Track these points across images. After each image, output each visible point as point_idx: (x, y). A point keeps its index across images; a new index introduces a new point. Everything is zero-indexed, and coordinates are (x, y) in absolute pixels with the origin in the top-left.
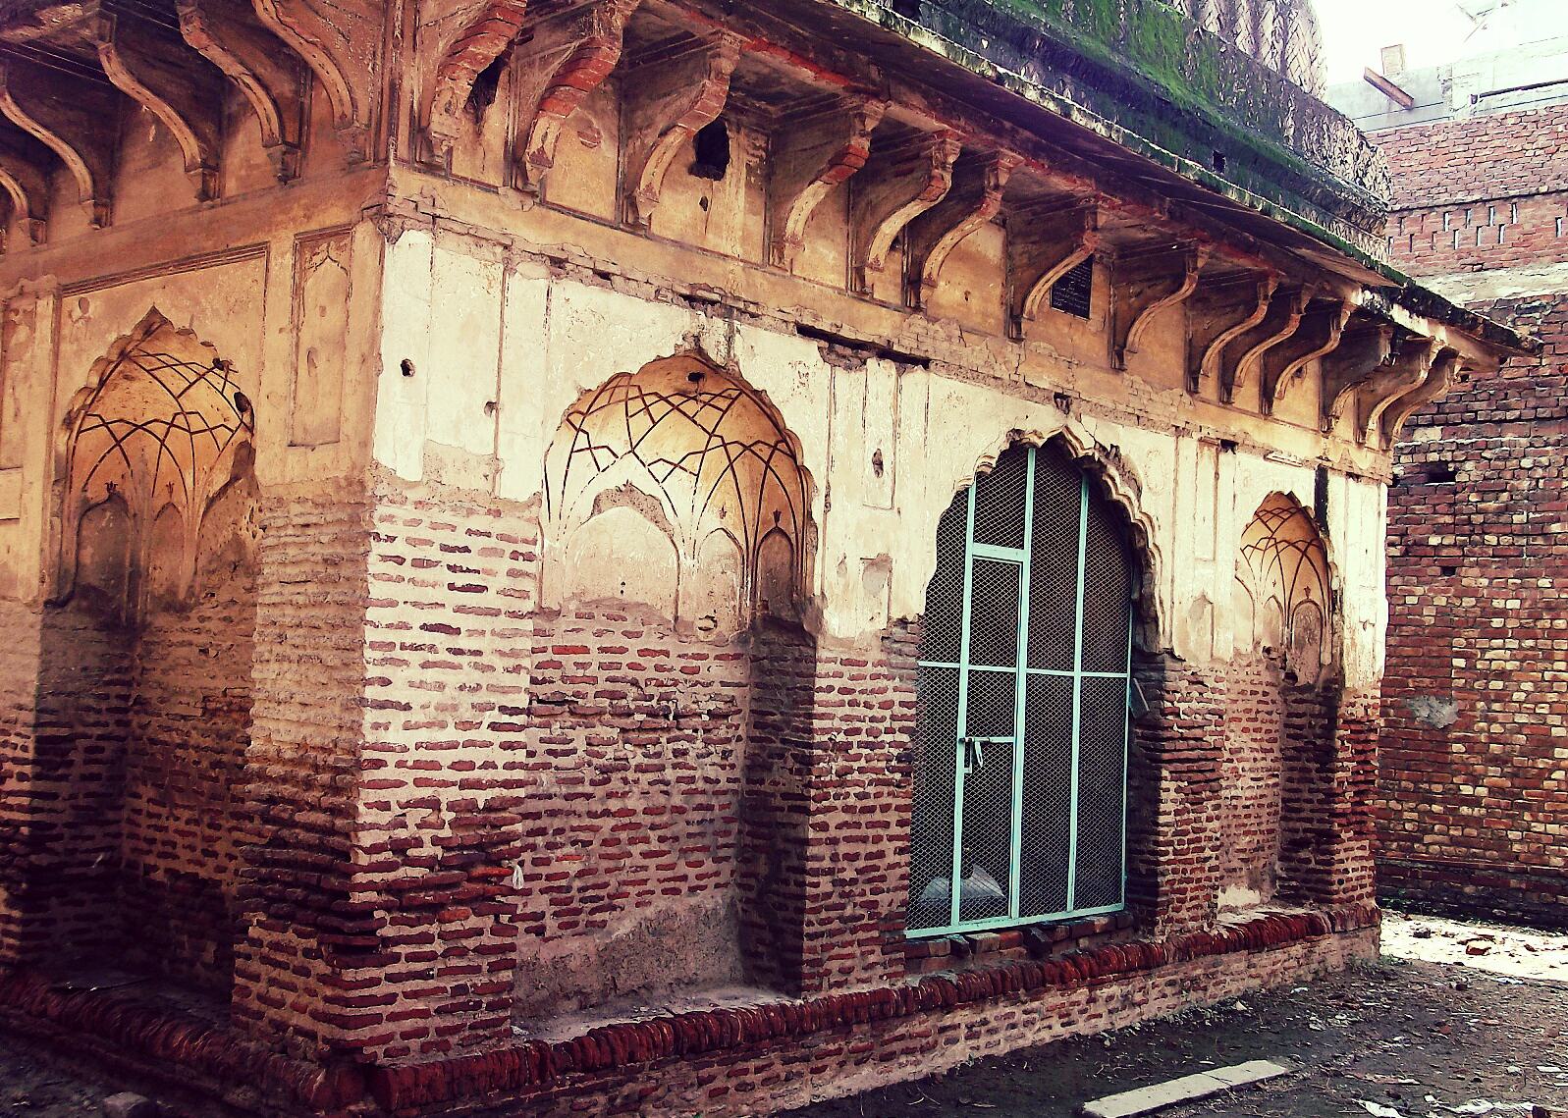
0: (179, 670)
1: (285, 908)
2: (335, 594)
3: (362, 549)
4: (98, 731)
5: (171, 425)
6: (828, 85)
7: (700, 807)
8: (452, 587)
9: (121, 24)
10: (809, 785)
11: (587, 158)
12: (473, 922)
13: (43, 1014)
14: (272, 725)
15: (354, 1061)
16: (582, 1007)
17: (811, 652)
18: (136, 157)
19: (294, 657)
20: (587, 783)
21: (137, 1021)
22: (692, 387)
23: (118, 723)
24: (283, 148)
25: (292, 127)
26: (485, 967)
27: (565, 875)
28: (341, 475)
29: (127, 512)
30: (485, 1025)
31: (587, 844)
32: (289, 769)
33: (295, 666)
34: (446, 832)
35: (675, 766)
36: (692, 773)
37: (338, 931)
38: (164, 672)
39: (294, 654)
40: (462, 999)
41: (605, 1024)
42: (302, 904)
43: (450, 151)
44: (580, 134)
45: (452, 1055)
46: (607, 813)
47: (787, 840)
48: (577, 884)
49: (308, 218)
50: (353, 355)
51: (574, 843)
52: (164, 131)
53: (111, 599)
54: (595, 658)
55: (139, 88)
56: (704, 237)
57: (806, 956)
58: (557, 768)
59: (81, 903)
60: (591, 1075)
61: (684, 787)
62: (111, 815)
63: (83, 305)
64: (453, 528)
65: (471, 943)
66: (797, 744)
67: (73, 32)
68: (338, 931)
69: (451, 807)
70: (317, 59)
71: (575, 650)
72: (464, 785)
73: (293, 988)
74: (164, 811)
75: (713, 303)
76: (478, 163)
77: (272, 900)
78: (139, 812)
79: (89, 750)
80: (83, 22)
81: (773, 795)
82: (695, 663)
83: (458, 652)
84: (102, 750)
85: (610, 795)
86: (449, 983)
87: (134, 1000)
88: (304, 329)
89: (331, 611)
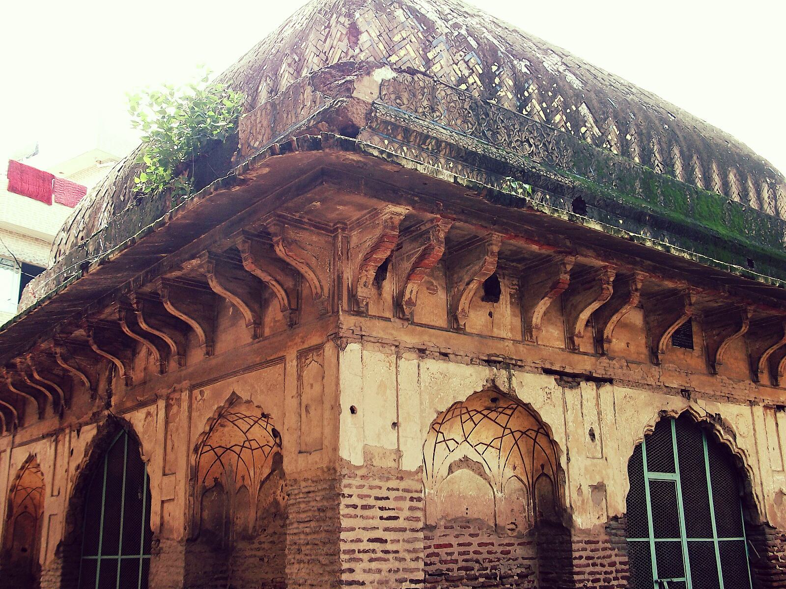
3: (336, 502)
5: (243, 447)
8: (381, 518)
18: (224, 322)
19: (306, 561)
22: (493, 405)
24: (290, 311)
33: (306, 565)
38: (243, 571)
43: (367, 304)
44: (428, 288)
50: (327, 406)
54: (456, 549)
56: (492, 331)
63: (202, 393)
64: (380, 488)
70: (303, 269)
76: (381, 308)
80: (200, 266)
82: (508, 548)
88: (303, 396)
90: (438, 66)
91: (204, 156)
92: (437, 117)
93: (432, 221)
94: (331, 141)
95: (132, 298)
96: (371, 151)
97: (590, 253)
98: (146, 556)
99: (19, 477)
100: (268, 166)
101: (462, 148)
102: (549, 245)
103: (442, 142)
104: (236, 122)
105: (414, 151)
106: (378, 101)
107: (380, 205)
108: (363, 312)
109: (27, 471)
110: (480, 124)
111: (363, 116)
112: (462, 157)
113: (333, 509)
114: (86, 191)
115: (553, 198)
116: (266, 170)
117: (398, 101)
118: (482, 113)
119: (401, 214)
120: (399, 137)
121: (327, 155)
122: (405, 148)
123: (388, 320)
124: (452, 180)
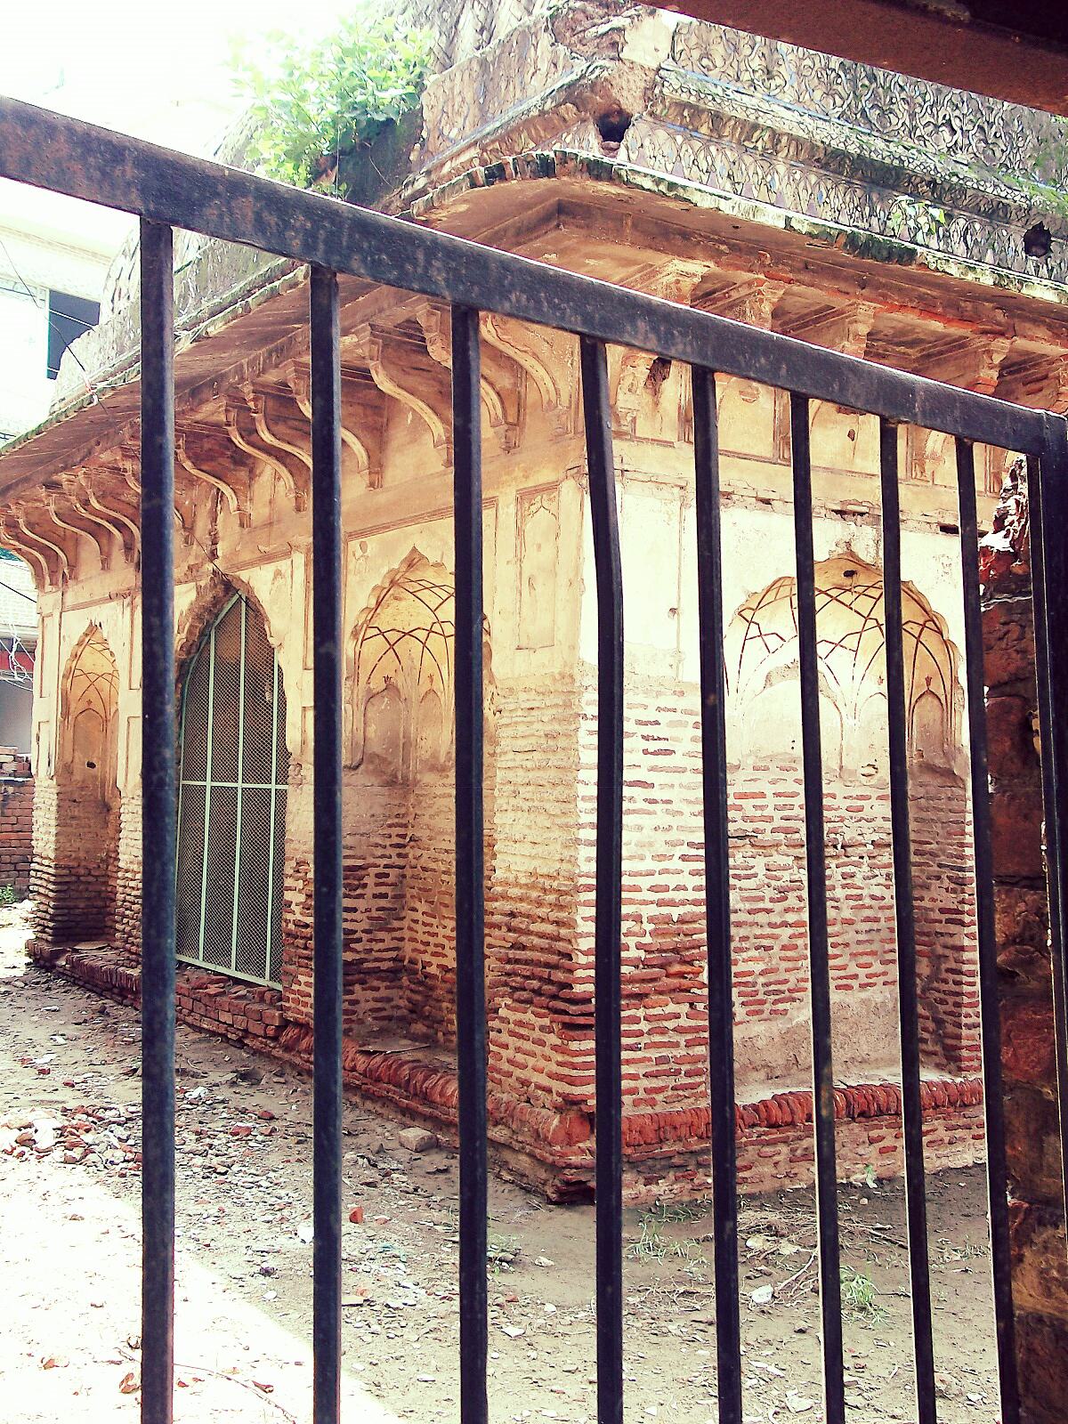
0: (442, 816)
1: (525, 995)
2: (554, 760)
3: (573, 727)
4: (386, 861)
5: (431, 631)
6: (956, 330)
7: (867, 919)
8: (646, 752)
9: (385, 346)
10: (963, 902)
11: (748, 409)
12: (672, 1008)
13: (353, 1069)
14: (510, 859)
15: (581, 1110)
16: (769, 1078)
17: (961, 792)
18: (398, 436)
19: (526, 808)
20: (767, 900)
21: (420, 1077)
22: (847, 582)
23: (399, 855)
24: (506, 427)
25: (512, 412)
26: (683, 1043)
27: (751, 973)
28: (556, 671)
29: (400, 697)
30: (685, 1087)
31: (768, 949)
32: (523, 891)
33: (526, 814)
34: (647, 940)
35: (844, 887)
36: (859, 892)
37: (565, 1012)
38: (431, 817)
39: (526, 805)
40: (665, 1067)
41: (787, 1091)
42: (538, 992)
43: (634, 420)
44: (741, 393)
45: (658, 1109)
46: (785, 924)
47: (945, 947)
48: (762, 980)
49: (527, 477)
50: (563, 580)
51: (757, 948)
52: (418, 418)
53: (390, 763)
54: (771, 801)
55: (400, 391)
56: (852, 462)
57: (964, 1043)
58: (741, 889)
59: (377, 989)
60: (775, 1130)
61: (852, 903)
62: (396, 924)
63: (363, 546)
64: (646, 707)
65: (671, 1024)
66: (952, 868)
67: (351, 351)
68: (565, 1012)
69: (651, 920)
70: (528, 362)
71: (754, 796)
72: (660, 903)
73: (533, 1055)
74: (434, 921)
75: (862, 514)
76: (657, 426)
77: (515, 989)
78: (416, 922)
79: (378, 876)
80: (358, 345)
81: (932, 910)
82: (860, 803)
83: (654, 802)
84: (387, 875)
85: (787, 910)
86: (654, 1054)
87: (418, 1061)
88: (524, 561)
89: (552, 774)
91: (363, 146)
92: (777, 87)
93: (750, 284)
94: (571, 164)
95: (246, 390)
96: (639, 180)
97: (1042, 332)
98: (279, 787)
99: (76, 656)
100: (465, 201)
101: (819, 144)
102: (962, 320)
104: (420, 86)
105: (728, 153)
106: (669, 64)
107: (658, 259)
108: (626, 434)
109: (88, 648)
111: (639, 93)
112: (818, 160)
113: (568, 736)
115: (988, 228)
116: (463, 208)
117: (705, 62)
119: (695, 275)
120: (704, 130)
121: (565, 183)
122: (713, 149)
123: (669, 444)
124: (781, 225)
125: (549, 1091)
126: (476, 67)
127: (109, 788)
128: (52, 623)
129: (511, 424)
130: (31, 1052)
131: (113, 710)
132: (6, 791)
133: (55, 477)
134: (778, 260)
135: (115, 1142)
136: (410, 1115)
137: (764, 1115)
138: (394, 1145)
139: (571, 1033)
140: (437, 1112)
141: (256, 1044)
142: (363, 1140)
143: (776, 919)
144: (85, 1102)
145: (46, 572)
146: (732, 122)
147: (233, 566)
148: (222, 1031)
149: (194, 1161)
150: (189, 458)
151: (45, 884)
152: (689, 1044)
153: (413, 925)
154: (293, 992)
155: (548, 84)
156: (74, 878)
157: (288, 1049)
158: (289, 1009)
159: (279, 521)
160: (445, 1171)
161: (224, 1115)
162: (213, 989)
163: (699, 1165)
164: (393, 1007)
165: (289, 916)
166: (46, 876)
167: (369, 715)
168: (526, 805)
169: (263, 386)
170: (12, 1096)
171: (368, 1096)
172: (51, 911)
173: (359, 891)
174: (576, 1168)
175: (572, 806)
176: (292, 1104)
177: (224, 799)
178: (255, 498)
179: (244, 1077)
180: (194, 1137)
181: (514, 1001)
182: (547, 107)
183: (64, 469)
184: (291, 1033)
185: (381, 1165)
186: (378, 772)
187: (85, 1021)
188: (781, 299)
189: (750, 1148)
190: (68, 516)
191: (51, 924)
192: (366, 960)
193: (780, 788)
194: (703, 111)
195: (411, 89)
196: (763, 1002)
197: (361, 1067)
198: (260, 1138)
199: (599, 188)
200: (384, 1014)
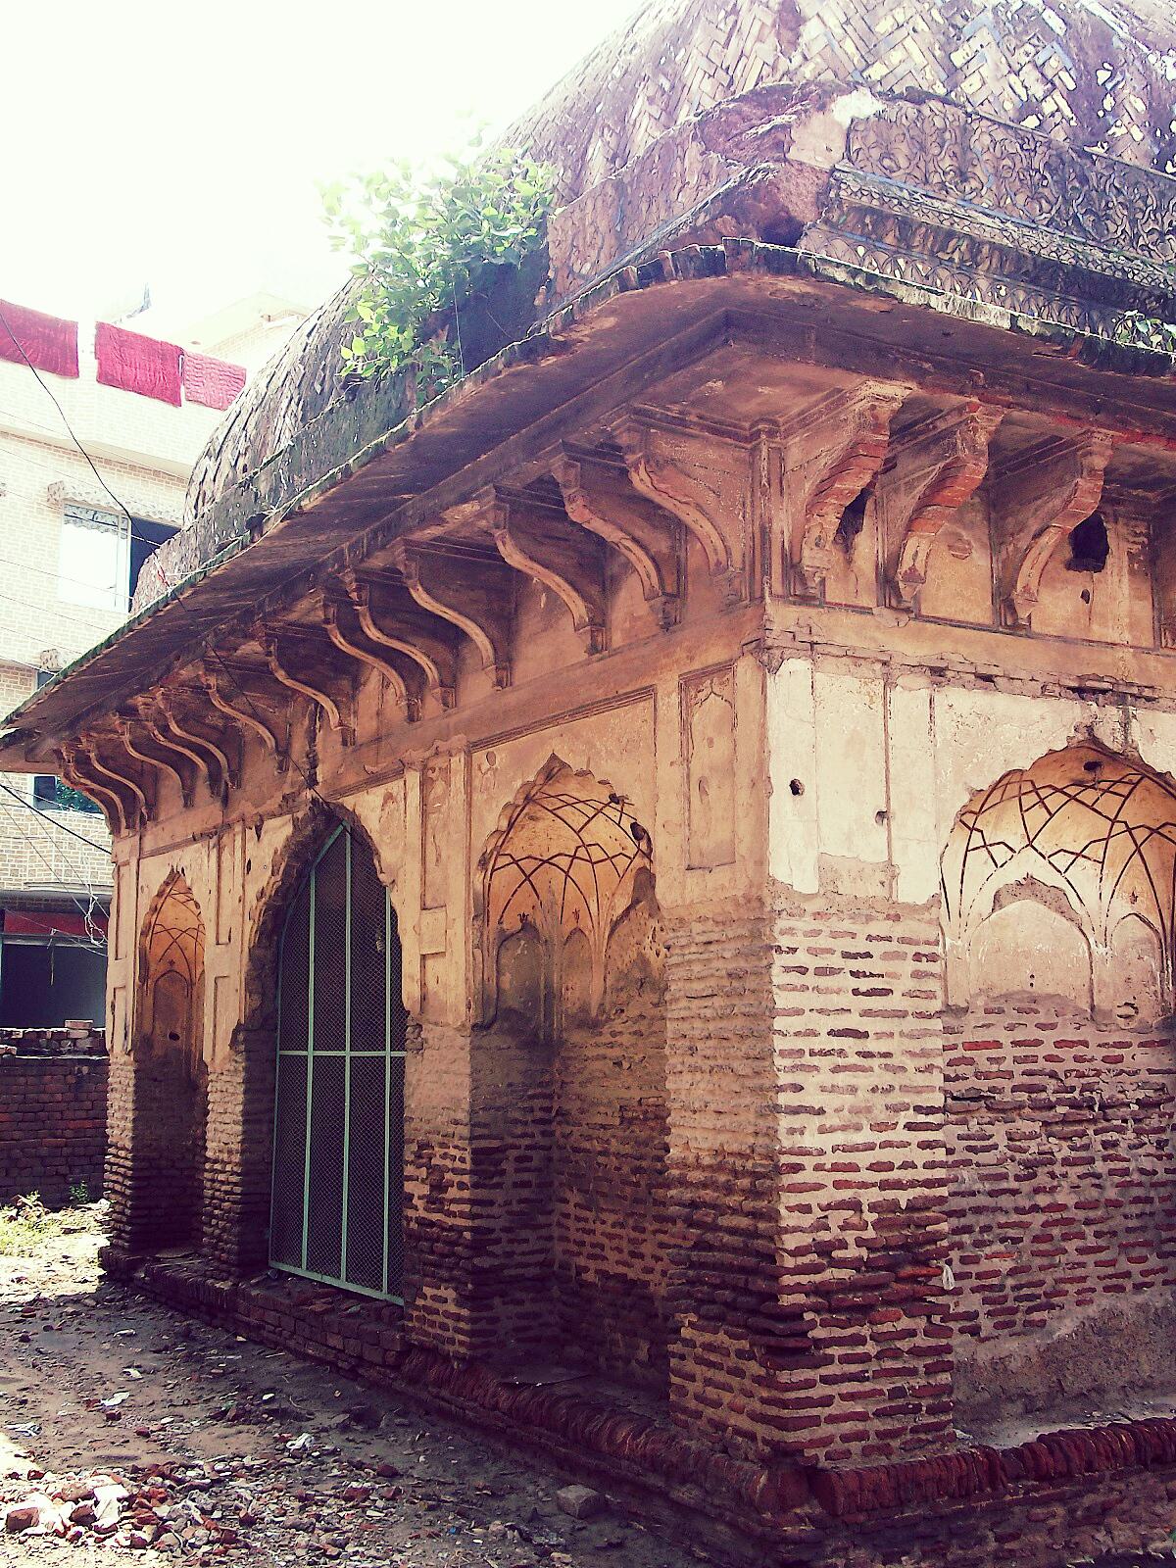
0: (595, 1083)
1: (714, 1309)
2: (740, 1006)
3: (765, 962)
4: (527, 1141)
5: (574, 857)
7: (1137, 1200)
8: (856, 992)
9: (513, 512)
11: (961, 567)
12: (905, 1323)
13: (495, 1407)
14: (688, 1133)
15: (796, 1463)
16: (1028, 1411)
18: (530, 623)
19: (707, 1068)
20: (1011, 1178)
21: (581, 1419)
22: (1089, 776)
24: (663, 599)
26: (922, 1370)
27: (996, 1273)
31: (1016, 1241)
33: (707, 1076)
34: (870, 1233)
35: (1105, 1159)
36: (1125, 1164)
39: (706, 1065)
40: (901, 1402)
42: (731, 1306)
43: (823, 581)
44: (950, 547)
45: (895, 1459)
46: (1035, 1208)
48: (1010, 1282)
50: (743, 779)
54: (1008, 1052)
56: (1088, 628)
58: (978, 1165)
61: (1117, 1179)
62: (541, 1219)
64: (853, 935)
65: (904, 1345)
69: (873, 1208)
70: (690, 517)
72: (884, 1185)
73: (729, 1388)
75: (1104, 692)
76: (852, 588)
77: (701, 1302)
78: (567, 1216)
79: (519, 1159)
80: (481, 515)
82: (1117, 1052)
84: (530, 1159)
85: (1037, 1191)
86: (886, 1386)
87: (577, 1395)
89: (739, 1023)
90: (975, 80)
93: (960, 410)
94: (746, 255)
96: (831, 271)
99: (155, 910)
103: (982, 243)
104: (541, 225)
105: (920, 267)
108: (814, 598)
110: (1067, 201)
111: (810, 199)
112: (1026, 273)
114: (244, 375)
116: (610, 322)
117: (887, 162)
118: (1073, 176)
120: (890, 239)
121: (737, 283)
122: (901, 262)
124: (1006, 324)
125: (752, 1437)
126: (610, 190)
127: (195, 1064)
128: (128, 873)
129: (668, 595)
130: (100, 1390)
131: (199, 971)
132: (80, 1071)
133: (130, 701)
134: (992, 380)
135: (197, 1515)
136: (568, 1470)
137: (1031, 1463)
138: (548, 1509)
139: (779, 1360)
140: (604, 1465)
141: (373, 1374)
142: (512, 1502)
143: (1023, 1202)
144: (161, 1459)
145: (122, 814)
146: (923, 230)
147: (336, 792)
148: (331, 1358)
149: (298, 1539)
150: (282, 667)
151: (121, 1179)
152: (930, 1371)
153: (563, 1221)
154: (417, 1308)
155: (699, 198)
156: (154, 1172)
157: (413, 1380)
158: (413, 1329)
159: (388, 736)
160: (620, 1546)
161: (335, 1472)
162: (318, 1306)
163: (952, 1534)
164: (541, 1325)
165: (410, 1213)
166: (122, 1170)
167: (503, 961)
168: (706, 1065)
169: (367, 573)
170: (71, 1452)
171: (513, 1443)
172: (128, 1212)
173: (495, 1180)
174: (795, 1543)
175: (767, 1063)
176: (419, 1454)
177: (329, 1070)
178: (360, 711)
179: (358, 1418)
180: (297, 1504)
181: (700, 1317)
182: (700, 222)
183: (139, 691)
184: (415, 1361)
185: (537, 1540)
186: (512, 1032)
187: (166, 1349)
188: (997, 431)
189: (1017, 1509)
190: (144, 745)
191: (128, 1228)
192: (507, 1267)
193: (1020, 1035)
194: (888, 217)
195: (532, 232)
196: (1014, 1311)
197: (504, 1404)
198: (380, 1504)
199: (781, 285)
200: (531, 1333)
